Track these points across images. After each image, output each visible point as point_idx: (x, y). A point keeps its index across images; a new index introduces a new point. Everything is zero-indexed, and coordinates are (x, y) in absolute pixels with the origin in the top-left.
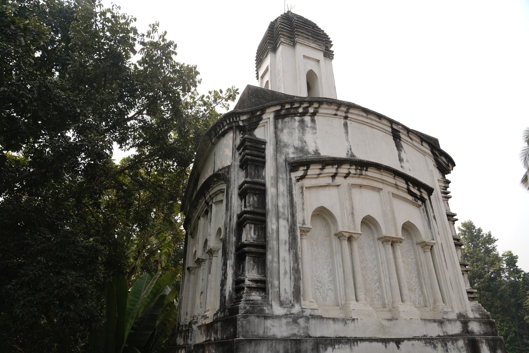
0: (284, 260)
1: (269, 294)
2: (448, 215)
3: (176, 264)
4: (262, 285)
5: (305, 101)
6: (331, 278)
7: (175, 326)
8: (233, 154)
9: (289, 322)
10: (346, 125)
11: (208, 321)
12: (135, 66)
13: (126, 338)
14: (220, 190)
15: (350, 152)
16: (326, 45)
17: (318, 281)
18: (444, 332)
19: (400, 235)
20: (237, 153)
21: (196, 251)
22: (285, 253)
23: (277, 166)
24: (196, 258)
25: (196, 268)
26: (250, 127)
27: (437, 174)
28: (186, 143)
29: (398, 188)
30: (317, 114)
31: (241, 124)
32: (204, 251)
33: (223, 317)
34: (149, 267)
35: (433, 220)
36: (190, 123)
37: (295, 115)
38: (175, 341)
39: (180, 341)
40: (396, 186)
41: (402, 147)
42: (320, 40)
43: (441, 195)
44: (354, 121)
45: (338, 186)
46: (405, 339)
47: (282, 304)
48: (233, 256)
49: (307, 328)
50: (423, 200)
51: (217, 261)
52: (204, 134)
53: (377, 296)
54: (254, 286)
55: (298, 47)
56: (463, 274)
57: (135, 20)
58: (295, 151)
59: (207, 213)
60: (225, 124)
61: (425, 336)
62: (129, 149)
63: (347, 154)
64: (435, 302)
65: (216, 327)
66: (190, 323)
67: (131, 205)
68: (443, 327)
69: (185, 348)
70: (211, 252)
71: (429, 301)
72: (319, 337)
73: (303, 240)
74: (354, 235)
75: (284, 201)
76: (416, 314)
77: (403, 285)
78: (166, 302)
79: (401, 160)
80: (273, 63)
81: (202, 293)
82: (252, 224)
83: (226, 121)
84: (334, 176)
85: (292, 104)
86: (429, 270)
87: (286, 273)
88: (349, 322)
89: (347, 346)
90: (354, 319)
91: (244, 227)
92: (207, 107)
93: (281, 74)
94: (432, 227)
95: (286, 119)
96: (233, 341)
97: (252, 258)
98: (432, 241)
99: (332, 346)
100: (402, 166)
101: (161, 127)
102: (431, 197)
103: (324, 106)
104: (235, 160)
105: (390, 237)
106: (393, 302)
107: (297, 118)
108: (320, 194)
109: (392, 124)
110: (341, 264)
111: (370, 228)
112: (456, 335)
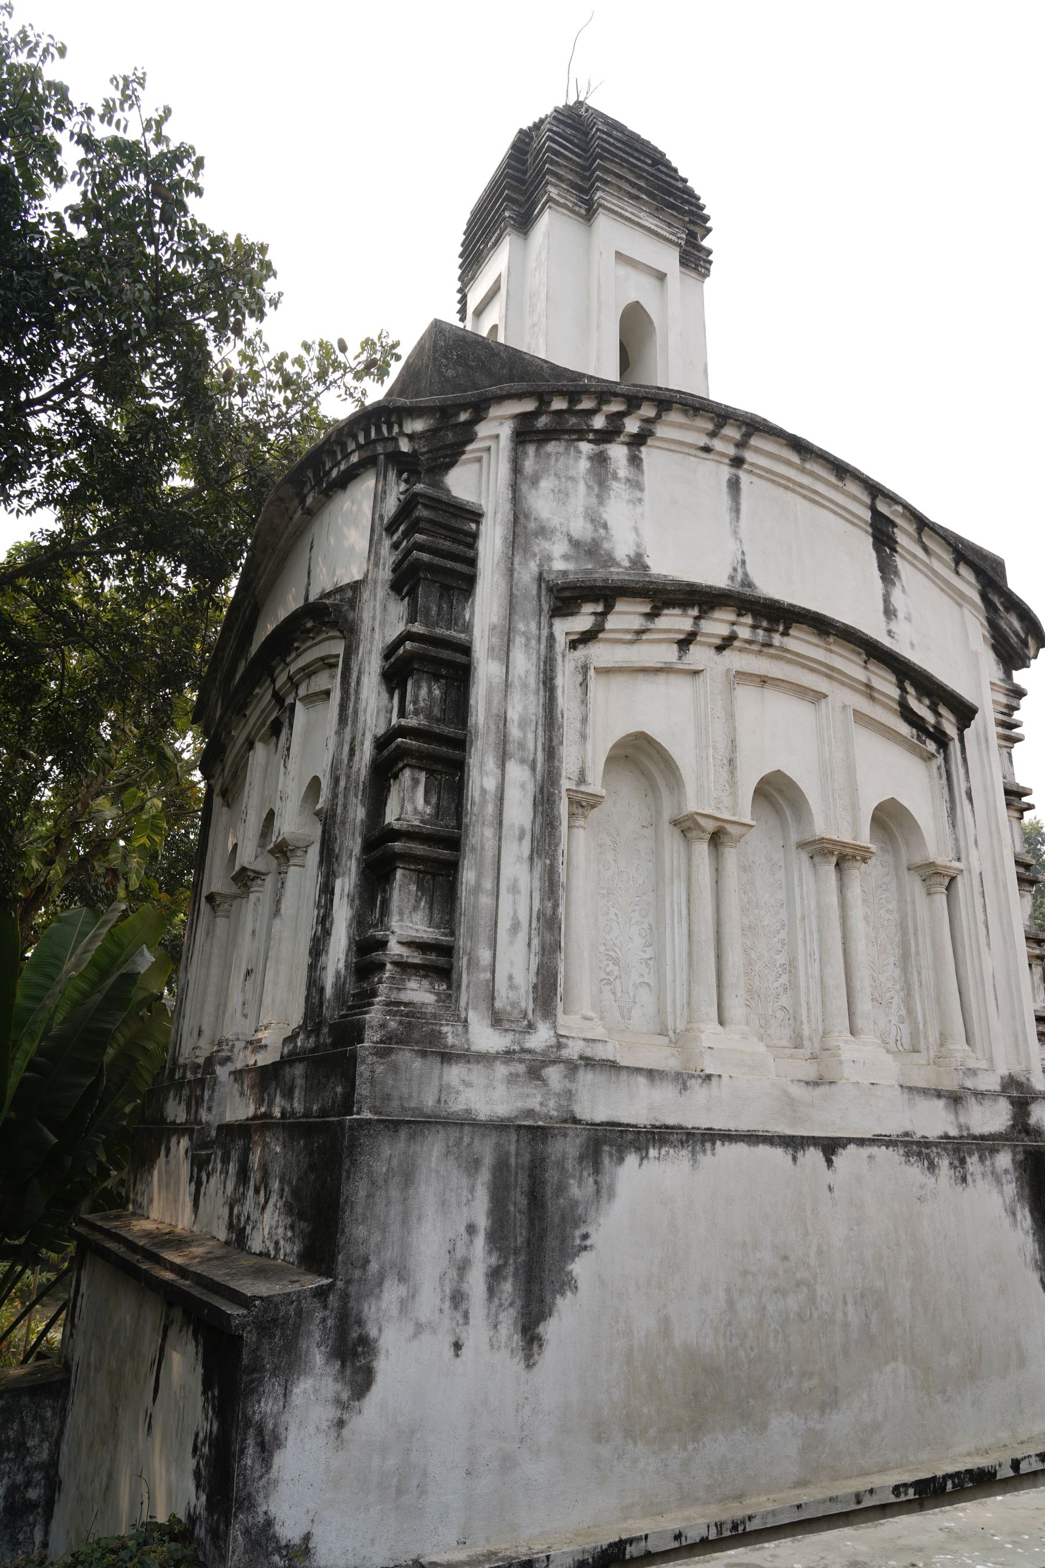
0: (514, 889)
1: (459, 987)
2: (1007, 792)
3: (172, 885)
4: (442, 961)
5: (616, 395)
6: (649, 953)
7: (164, 1067)
8: (374, 544)
9: (517, 1075)
10: (734, 485)
11: (264, 1059)
12: (59, 221)
13: (10, 1093)
14: (322, 659)
15: (740, 571)
16: (692, 227)
17: (610, 958)
18: (960, 1127)
19: (865, 838)
20: (387, 543)
21: (235, 846)
22: (517, 867)
23: (511, 595)
24: (237, 868)
25: (235, 897)
26: (435, 459)
27: (990, 666)
28: (221, 503)
29: (872, 698)
30: (650, 442)
31: (405, 446)
32: (262, 845)
33: (313, 1050)
34: (87, 888)
35: (966, 802)
36: (237, 441)
37: (581, 434)
38: (161, 1110)
39: (176, 1111)
40: (869, 691)
41: (896, 573)
42: (673, 207)
43: (994, 730)
44: (760, 476)
45: (696, 673)
47: (497, 1020)
48: (353, 866)
49: (569, 1094)
50: (941, 740)
51: (303, 879)
52: (278, 479)
53: (780, 1014)
54: (417, 961)
55: (602, 220)
56: (1030, 965)
57: (62, 51)
58: (571, 552)
59: (276, 729)
60: (351, 446)
61: (907, 1134)
62: (33, 509)
63: (732, 578)
64: (943, 1039)
65: (288, 1077)
66: (210, 1061)
67: (36, 691)
68: (961, 1112)
69: (190, 1132)
70: (283, 852)
71: (926, 1037)
72: (602, 1124)
73: (575, 831)
74: (730, 828)
75: (525, 707)
76: (889, 1070)
77: (857, 985)
78: (138, 995)
79: (889, 612)
80: (517, 267)
81: (248, 973)
82: (421, 769)
83: (355, 437)
84: (685, 642)
85: (573, 396)
86: (936, 948)
87: (515, 927)
89: (684, 1152)
90: (709, 1077)
91: (396, 777)
92: (294, 392)
93: (541, 305)
94: (959, 823)
95: (552, 447)
96: (341, 1124)
97: (414, 877)
98: (956, 864)
99: (638, 1149)
100: (890, 633)
101: (140, 441)
102: (967, 732)
103: (674, 416)
104: (376, 565)
105: (835, 842)
106: (825, 1034)
107: (585, 447)
108: (637, 692)
109: (874, 498)
110: (684, 911)
111: (778, 811)
112: (992, 1137)
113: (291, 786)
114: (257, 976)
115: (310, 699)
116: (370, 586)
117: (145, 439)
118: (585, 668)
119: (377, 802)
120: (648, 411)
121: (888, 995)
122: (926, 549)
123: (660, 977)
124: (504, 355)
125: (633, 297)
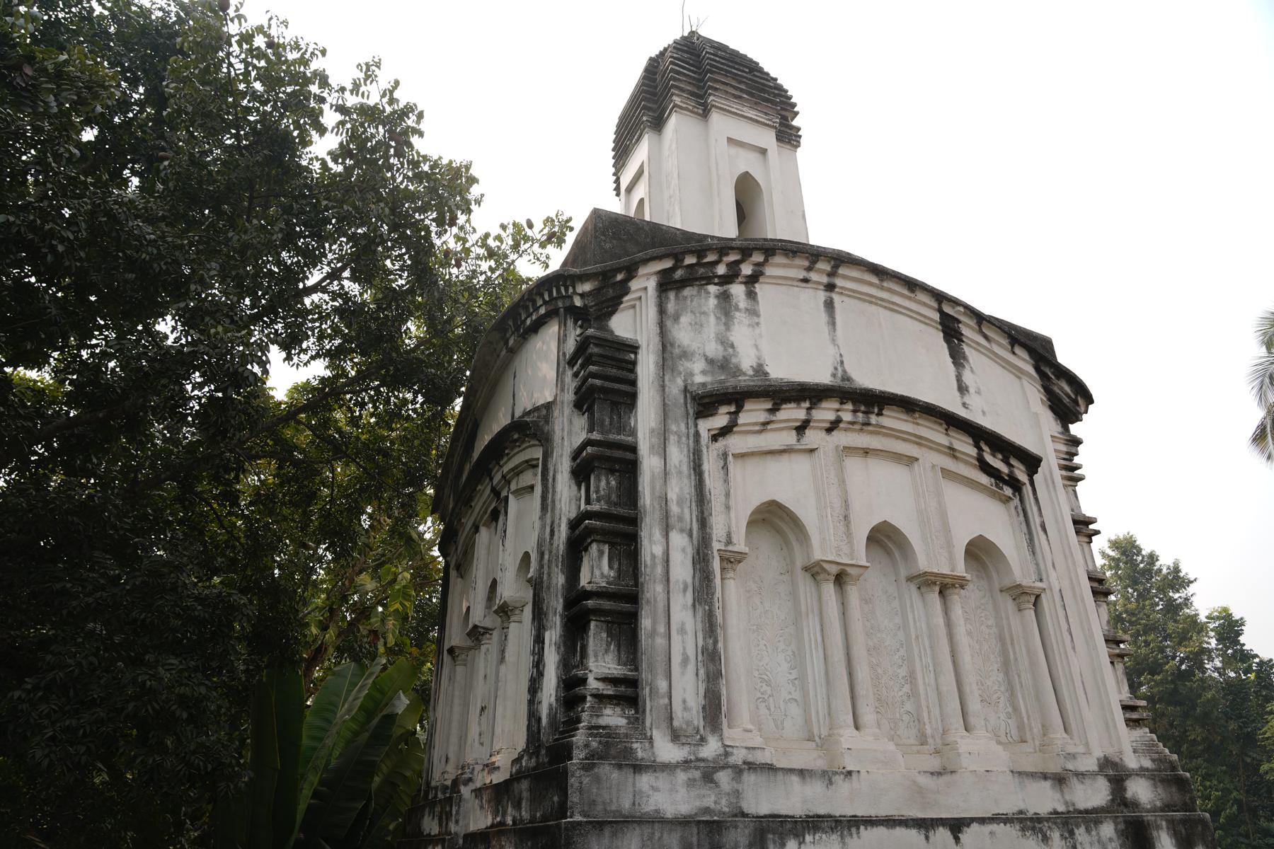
0: (682, 631)
1: (644, 711)
2: (1075, 522)
3: (421, 640)
4: (630, 691)
5: (732, 249)
6: (795, 674)
7: (419, 790)
9: (695, 780)
10: (829, 305)
11: (497, 778)
12: (324, 163)
13: (299, 817)
14: (527, 461)
15: (840, 369)
16: (783, 113)
17: (763, 681)
18: (1066, 803)
19: (961, 569)
20: (569, 373)
22: (683, 614)
24: (470, 626)
25: (470, 649)
26: (600, 310)
27: (1049, 423)
28: (446, 349)
29: (955, 457)
30: (761, 279)
31: (578, 302)
32: (488, 607)
33: (535, 768)
34: (355, 646)
36: (456, 301)
37: (709, 280)
38: (419, 825)
40: (952, 452)
41: (965, 358)
43: (1058, 474)
45: (812, 451)
46: (973, 820)
47: (676, 736)
48: (558, 620)
49: (737, 793)
50: (1016, 486)
51: (521, 631)
53: (906, 717)
54: (610, 692)
55: (715, 117)
57: (324, 52)
58: (708, 368)
59: (495, 516)
60: (540, 302)
61: (1021, 812)
63: (834, 375)
64: (1045, 730)
65: (516, 791)
66: (455, 782)
67: (313, 496)
70: (505, 612)
71: (1031, 729)
74: (849, 570)
75: (681, 489)
76: (1000, 758)
77: (967, 689)
78: (397, 732)
79: (962, 389)
80: (654, 156)
81: (483, 709)
82: (605, 542)
83: (542, 296)
84: (801, 428)
85: (700, 254)
87: (685, 660)
88: (838, 779)
89: (834, 837)
90: (850, 773)
91: (586, 550)
92: (496, 261)
93: (675, 182)
95: (687, 292)
96: (558, 826)
97: (604, 626)
99: (796, 836)
100: (964, 405)
102: (1035, 477)
103: (779, 259)
104: (562, 390)
105: (936, 575)
106: (944, 732)
107: (713, 289)
108: (768, 469)
110: (819, 639)
111: (888, 552)
113: (509, 560)
114: (489, 711)
115: (520, 492)
116: (559, 406)
117: (389, 306)
118: (725, 455)
119: (573, 571)
120: (758, 257)
121: (995, 696)
122: (986, 337)
123: (805, 695)
124: (647, 228)
125: (743, 169)
